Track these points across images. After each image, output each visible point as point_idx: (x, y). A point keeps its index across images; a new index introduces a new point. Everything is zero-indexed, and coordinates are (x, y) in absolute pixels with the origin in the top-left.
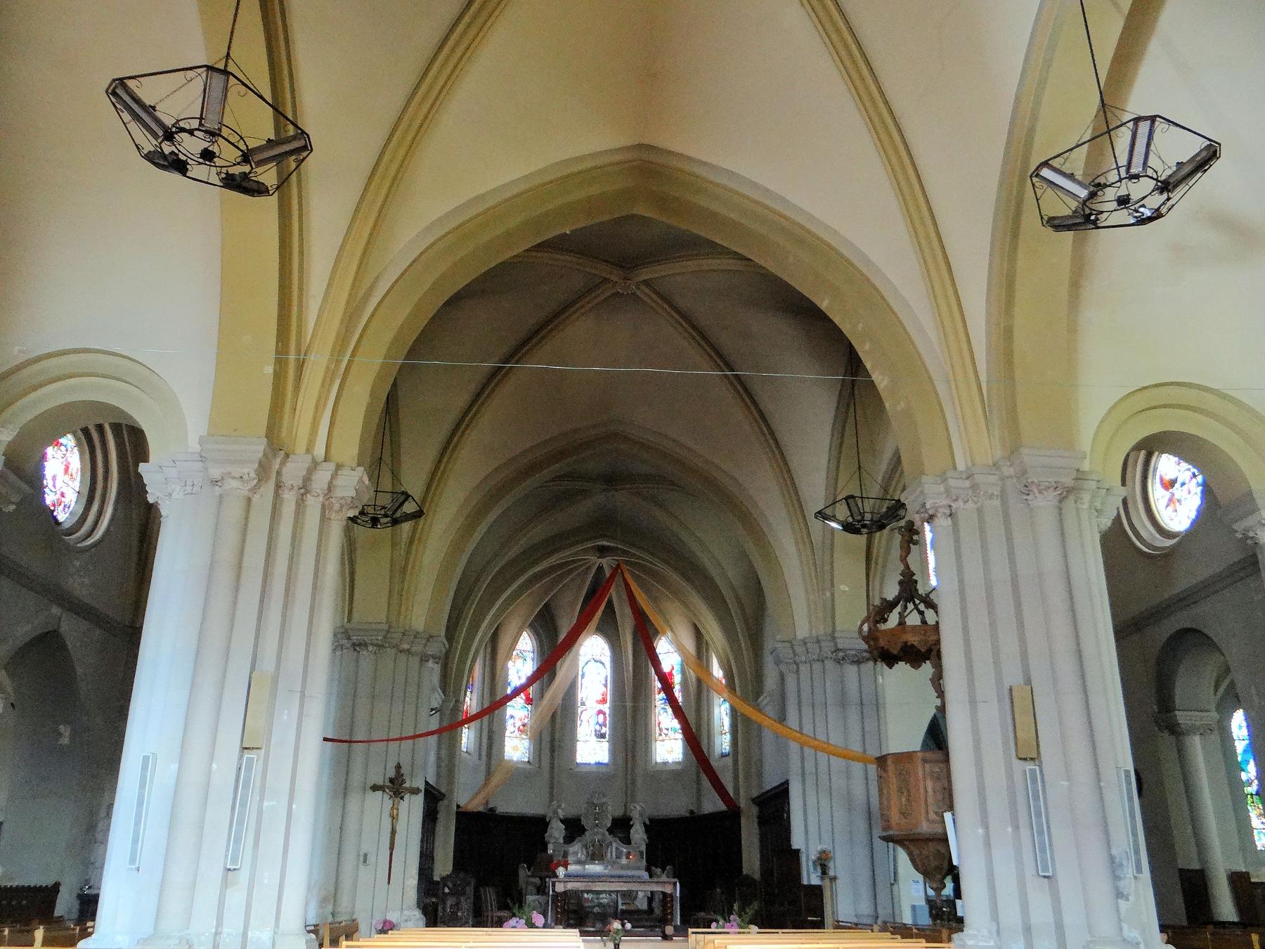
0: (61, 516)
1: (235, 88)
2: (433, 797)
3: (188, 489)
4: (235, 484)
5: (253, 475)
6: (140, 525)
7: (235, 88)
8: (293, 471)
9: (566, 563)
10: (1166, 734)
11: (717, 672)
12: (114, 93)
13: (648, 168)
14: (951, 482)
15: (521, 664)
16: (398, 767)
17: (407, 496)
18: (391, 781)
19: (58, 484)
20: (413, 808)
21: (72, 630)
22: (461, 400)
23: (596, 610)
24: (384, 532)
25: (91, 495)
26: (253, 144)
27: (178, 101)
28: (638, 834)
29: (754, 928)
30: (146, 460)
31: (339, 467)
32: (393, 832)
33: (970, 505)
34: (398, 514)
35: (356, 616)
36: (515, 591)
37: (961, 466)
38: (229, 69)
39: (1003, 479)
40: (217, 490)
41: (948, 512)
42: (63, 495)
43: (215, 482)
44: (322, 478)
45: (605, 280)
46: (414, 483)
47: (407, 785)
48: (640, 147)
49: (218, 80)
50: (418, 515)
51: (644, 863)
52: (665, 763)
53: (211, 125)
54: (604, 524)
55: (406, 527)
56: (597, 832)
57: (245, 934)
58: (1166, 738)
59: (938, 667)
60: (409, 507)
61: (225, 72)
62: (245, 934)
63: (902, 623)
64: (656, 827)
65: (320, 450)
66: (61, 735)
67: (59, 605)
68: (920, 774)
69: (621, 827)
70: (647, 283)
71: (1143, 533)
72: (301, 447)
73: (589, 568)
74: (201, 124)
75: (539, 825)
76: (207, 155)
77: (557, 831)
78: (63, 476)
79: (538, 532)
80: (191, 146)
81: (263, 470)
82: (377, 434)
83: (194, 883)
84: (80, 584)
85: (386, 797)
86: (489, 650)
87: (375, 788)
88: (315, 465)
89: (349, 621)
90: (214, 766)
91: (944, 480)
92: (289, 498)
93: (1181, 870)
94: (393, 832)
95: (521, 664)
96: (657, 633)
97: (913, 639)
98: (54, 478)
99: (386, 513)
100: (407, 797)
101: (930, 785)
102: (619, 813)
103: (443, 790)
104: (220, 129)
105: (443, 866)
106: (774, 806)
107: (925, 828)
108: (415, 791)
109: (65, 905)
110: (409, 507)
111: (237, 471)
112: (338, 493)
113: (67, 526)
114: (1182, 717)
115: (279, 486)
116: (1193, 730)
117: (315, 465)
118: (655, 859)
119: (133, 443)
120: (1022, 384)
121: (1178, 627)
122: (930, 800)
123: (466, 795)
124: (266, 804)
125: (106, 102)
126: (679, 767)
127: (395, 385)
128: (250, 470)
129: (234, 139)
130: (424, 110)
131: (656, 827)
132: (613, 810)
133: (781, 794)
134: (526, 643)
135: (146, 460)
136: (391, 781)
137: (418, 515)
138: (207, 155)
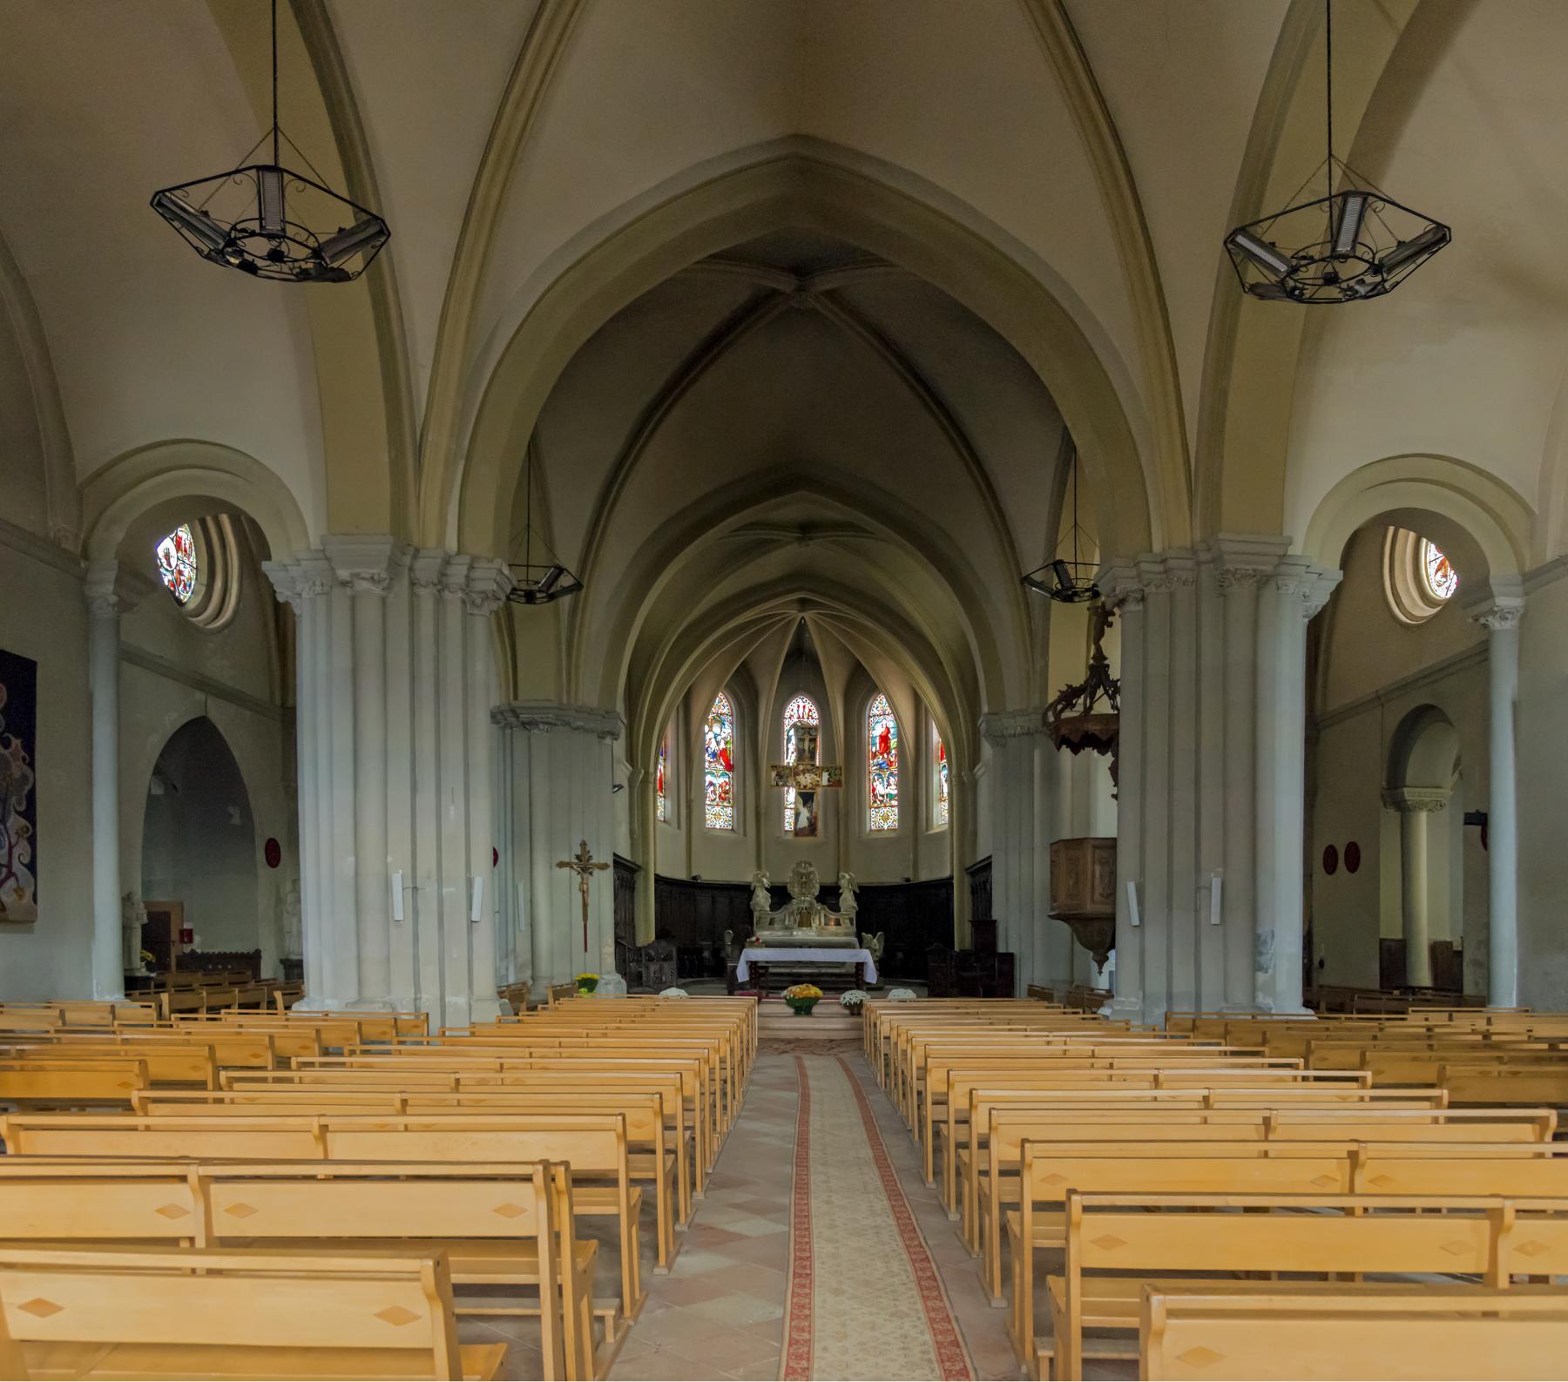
0: (184, 596)
1: (292, 186)
2: (626, 873)
3: (318, 588)
4: (365, 585)
5: (383, 575)
6: (279, 624)
7: (292, 186)
8: (426, 568)
9: (771, 616)
10: (1391, 811)
11: (936, 738)
12: (160, 204)
13: (808, 168)
14: (1144, 566)
15: (719, 734)
16: (583, 844)
17: (560, 571)
18: (578, 857)
19: (173, 562)
20: (603, 884)
21: (222, 716)
22: (613, 447)
23: (801, 668)
24: (543, 608)
25: (209, 570)
26: (322, 239)
27: (233, 204)
28: (848, 900)
29: (925, 991)
30: (269, 558)
31: (474, 559)
32: (585, 905)
33: (1163, 589)
34: (552, 590)
35: (520, 694)
36: (713, 643)
37: (1157, 547)
38: (281, 165)
39: (1198, 564)
40: (349, 591)
41: (1139, 596)
42: (180, 573)
43: (344, 584)
44: (458, 573)
45: (774, 293)
46: (569, 557)
47: (593, 861)
48: (796, 137)
49: (271, 180)
50: (577, 587)
51: (854, 929)
52: (880, 830)
53: (274, 227)
54: (798, 580)
55: (566, 600)
56: (803, 899)
57: (442, 998)
58: (1391, 816)
59: (1116, 755)
60: (566, 581)
61: (275, 168)
62: (442, 998)
63: (1088, 709)
64: (865, 895)
65: (452, 544)
66: (231, 816)
67: (201, 690)
68: (1089, 859)
69: (829, 895)
70: (831, 294)
71: (1405, 600)
72: (431, 542)
73: (789, 624)
74: (261, 227)
75: (746, 891)
76: (276, 256)
77: (762, 899)
78: (177, 557)
79: (728, 586)
80: (257, 247)
81: (393, 565)
82: (519, 484)
83: (388, 959)
84: (218, 668)
85: (574, 873)
86: (681, 714)
87: (561, 865)
88: (447, 561)
89: (516, 698)
90: (390, 859)
91: (1136, 565)
92: (426, 594)
93: (1382, 941)
94: (585, 905)
95: (719, 734)
96: (873, 689)
97: (1093, 728)
98: (167, 556)
99: (538, 590)
100: (596, 872)
101: (1098, 868)
102: (829, 880)
103: (639, 862)
104: (283, 230)
105: (646, 933)
106: (980, 874)
107: (1090, 908)
108: (604, 867)
109: (269, 968)
110: (566, 581)
111: (366, 572)
112: (479, 586)
113: (191, 606)
114: (1409, 794)
115: (413, 584)
116: (1421, 806)
117: (447, 561)
118: (864, 924)
119: (254, 546)
120: (1235, 446)
121: (1413, 706)
122: (1097, 882)
123: (666, 860)
124: (445, 890)
125: (154, 216)
126: (893, 835)
127: (536, 427)
128: (379, 571)
129: (303, 236)
130: (522, 115)
131: (865, 895)
132: (819, 878)
133: (986, 866)
134: (722, 705)
135: (269, 558)
136: (578, 857)
137: (577, 587)
138: (276, 256)
